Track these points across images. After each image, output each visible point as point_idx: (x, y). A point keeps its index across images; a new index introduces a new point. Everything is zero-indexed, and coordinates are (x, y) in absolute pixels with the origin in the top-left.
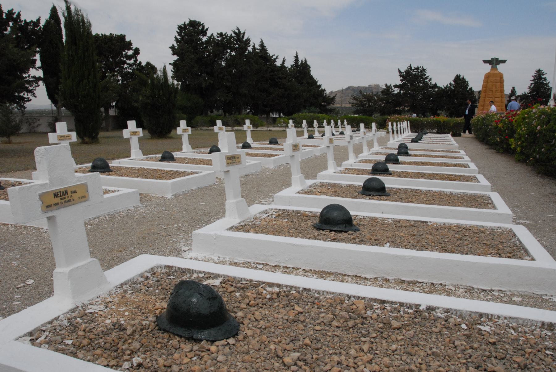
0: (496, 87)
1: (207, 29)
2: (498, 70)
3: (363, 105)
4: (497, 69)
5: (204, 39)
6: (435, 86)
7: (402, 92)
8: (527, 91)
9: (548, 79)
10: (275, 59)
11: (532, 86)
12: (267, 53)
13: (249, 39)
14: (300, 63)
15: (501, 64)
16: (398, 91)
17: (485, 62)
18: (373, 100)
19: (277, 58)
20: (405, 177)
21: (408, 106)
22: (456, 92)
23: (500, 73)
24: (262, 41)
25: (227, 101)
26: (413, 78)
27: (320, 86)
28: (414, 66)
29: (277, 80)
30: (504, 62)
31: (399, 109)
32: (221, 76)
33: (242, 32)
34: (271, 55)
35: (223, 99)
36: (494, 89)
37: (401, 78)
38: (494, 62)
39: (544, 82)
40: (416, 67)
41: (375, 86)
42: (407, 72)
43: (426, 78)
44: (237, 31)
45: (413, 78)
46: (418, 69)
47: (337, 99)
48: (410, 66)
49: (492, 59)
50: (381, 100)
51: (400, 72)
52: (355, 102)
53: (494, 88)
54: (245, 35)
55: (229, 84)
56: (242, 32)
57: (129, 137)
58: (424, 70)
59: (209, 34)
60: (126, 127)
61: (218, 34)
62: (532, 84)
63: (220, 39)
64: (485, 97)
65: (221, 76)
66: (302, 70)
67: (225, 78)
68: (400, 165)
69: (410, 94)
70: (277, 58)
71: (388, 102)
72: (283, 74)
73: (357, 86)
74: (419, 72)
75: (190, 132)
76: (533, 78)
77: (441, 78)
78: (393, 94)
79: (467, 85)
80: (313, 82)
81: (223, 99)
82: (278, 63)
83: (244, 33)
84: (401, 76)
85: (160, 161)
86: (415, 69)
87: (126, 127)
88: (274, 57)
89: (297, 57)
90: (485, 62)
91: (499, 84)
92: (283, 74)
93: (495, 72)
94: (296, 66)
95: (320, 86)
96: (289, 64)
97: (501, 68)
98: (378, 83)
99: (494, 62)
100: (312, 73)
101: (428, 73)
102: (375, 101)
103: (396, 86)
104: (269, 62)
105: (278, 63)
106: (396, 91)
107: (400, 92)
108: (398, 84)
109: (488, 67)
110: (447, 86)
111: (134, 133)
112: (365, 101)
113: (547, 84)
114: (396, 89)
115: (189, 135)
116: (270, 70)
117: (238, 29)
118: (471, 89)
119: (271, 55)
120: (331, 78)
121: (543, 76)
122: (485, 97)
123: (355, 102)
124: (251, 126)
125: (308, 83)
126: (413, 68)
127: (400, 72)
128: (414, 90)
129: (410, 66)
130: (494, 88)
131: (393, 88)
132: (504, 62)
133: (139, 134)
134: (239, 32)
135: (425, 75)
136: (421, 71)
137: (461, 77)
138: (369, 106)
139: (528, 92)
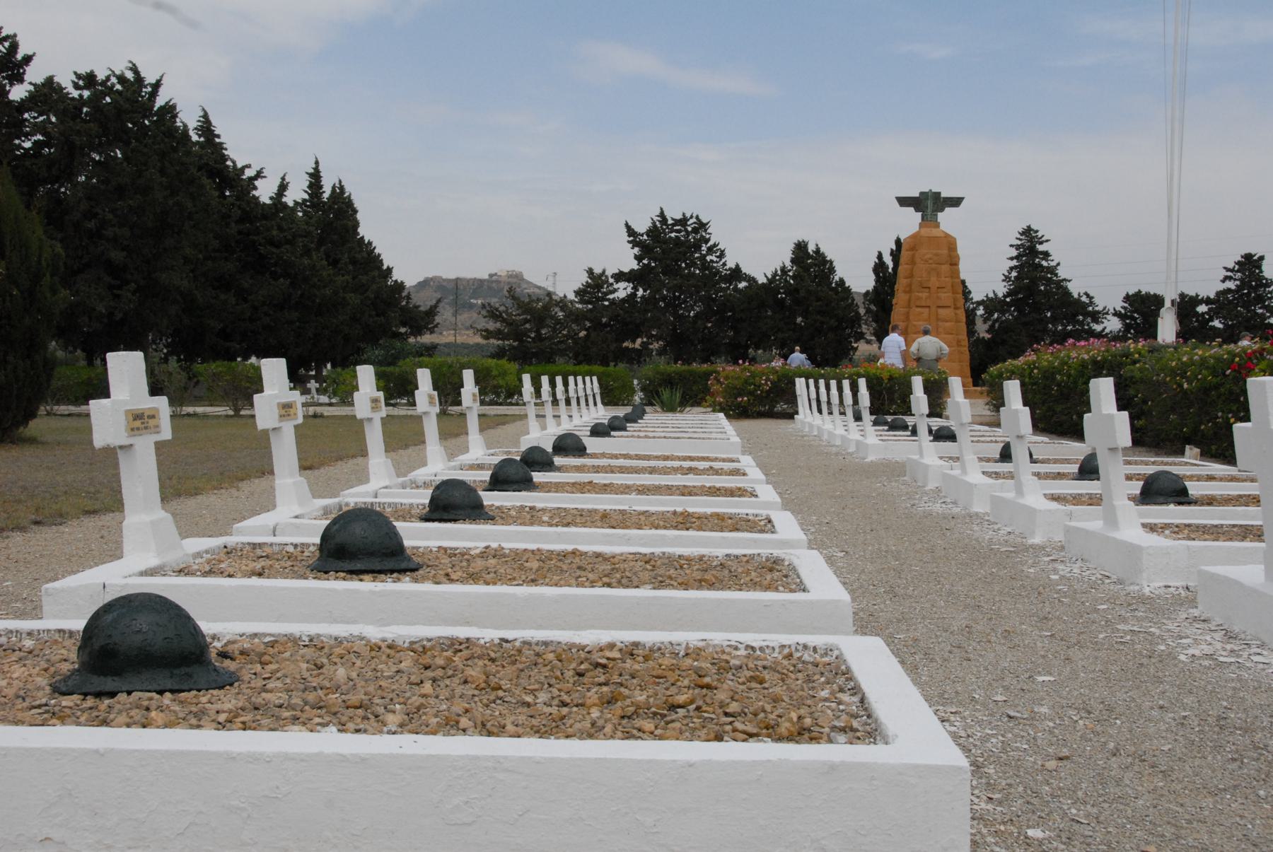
0: (938, 275)
1: (28, 59)
2: (942, 227)
3: (519, 335)
4: (937, 225)
5: (18, 93)
6: (737, 273)
7: (640, 292)
8: (1001, 289)
9: (1056, 257)
10: (252, 179)
11: (1014, 274)
12: (224, 158)
13: (174, 107)
14: (326, 196)
15: (947, 210)
16: (629, 290)
17: (904, 202)
18: (553, 317)
19: (259, 175)
20: (1210, 504)
21: (658, 338)
22: (802, 293)
23: (947, 236)
24: (206, 116)
25: (119, 316)
26: (672, 250)
27: (389, 270)
28: (673, 214)
29: (262, 250)
30: (956, 202)
31: (631, 346)
32: (91, 225)
33: (150, 78)
34: (239, 165)
35: (101, 308)
36: (934, 282)
37: (636, 250)
38: (929, 204)
39: (1044, 263)
40: (679, 217)
41: (510, 276)
42: (653, 232)
43: (710, 250)
44: (130, 75)
45: (672, 250)
46: (683, 221)
47: (445, 315)
48: (662, 215)
49: (921, 193)
50: (577, 317)
51: (631, 231)
52: (492, 325)
53: (934, 279)
54: (162, 91)
55: (117, 256)
56: (150, 78)
57: (123, 440)
58: (702, 226)
59: (35, 74)
60: (102, 390)
61: (79, 76)
62: (1012, 269)
63: (86, 94)
64: (909, 306)
65: (91, 225)
66: (332, 215)
67: (109, 232)
68: (406, 586)
69: (664, 298)
70: (259, 175)
71: (598, 326)
72: (280, 229)
73: (452, 276)
74: (688, 233)
75: (166, 433)
76: (1014, 253)
77: (755, 252)
78: (613, 302)
79: (832, 270)
80: (368, 261)
81: (101, 308)
82: (265, 192)
83: (157, 85)
84: (635, 244)
85: (427, 519)
86: (677, 222)
87: (102, 390)
88: (249, 173)
89: (315, 176)
90: (904, 202)
91: (945, 268)
92: (280, 229)
93: (934, 232)
94: (312, 206)
95: (389, 270)
96: (297, 193)
97: (948, 220)
98: (518, 269)
99: (930, 203)
100: (365, 231)
101: (716, 235)
102: (558, 322)
103: (620, 276)
104: (231, 188)
105: (265, 192)
106: (623, 290)
107: (633, 295)
108: (626, 270)
109: (910, 222)
110: (775, 274)
111: (287, 407)
112: (526, 321)
113: (1052, 270)
114: (622, 285)
115: (159, 446)
116: (237, 213)
117: (135, 69)
118: (842, 282)
119: (239, 165)
120: (413, 243)
121: (1040, 248)
122: (909, 306)
123: (492, 325)
124: (381, 394)
125: (354, 262)
126: (670, 222)
127: (631, 231)
128: (679, 288)
129: (662, 215)
130: (934, 279)
131: (611, 280)
132: (956, 202)
133: (157, 430)
134: (139, 79)
135: (707, 241)
136: (695, 231)
137: (811, 248)
138: (539, 338)
139: (1005, 290)
